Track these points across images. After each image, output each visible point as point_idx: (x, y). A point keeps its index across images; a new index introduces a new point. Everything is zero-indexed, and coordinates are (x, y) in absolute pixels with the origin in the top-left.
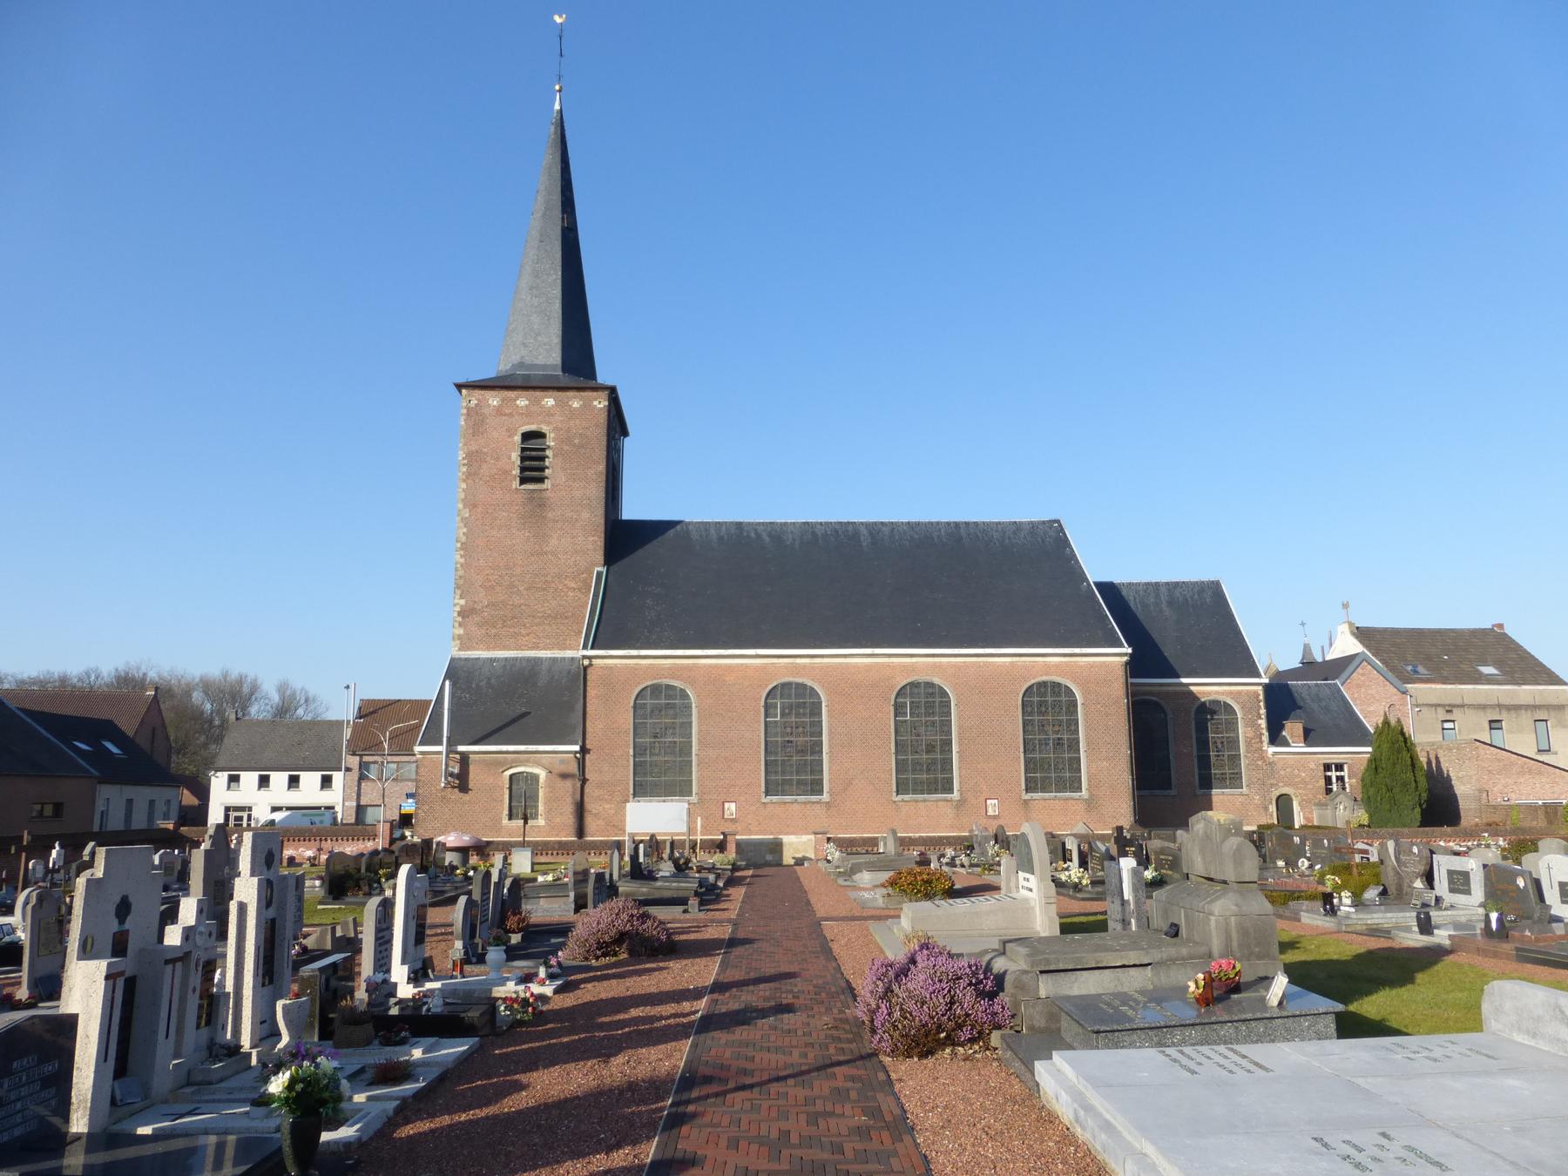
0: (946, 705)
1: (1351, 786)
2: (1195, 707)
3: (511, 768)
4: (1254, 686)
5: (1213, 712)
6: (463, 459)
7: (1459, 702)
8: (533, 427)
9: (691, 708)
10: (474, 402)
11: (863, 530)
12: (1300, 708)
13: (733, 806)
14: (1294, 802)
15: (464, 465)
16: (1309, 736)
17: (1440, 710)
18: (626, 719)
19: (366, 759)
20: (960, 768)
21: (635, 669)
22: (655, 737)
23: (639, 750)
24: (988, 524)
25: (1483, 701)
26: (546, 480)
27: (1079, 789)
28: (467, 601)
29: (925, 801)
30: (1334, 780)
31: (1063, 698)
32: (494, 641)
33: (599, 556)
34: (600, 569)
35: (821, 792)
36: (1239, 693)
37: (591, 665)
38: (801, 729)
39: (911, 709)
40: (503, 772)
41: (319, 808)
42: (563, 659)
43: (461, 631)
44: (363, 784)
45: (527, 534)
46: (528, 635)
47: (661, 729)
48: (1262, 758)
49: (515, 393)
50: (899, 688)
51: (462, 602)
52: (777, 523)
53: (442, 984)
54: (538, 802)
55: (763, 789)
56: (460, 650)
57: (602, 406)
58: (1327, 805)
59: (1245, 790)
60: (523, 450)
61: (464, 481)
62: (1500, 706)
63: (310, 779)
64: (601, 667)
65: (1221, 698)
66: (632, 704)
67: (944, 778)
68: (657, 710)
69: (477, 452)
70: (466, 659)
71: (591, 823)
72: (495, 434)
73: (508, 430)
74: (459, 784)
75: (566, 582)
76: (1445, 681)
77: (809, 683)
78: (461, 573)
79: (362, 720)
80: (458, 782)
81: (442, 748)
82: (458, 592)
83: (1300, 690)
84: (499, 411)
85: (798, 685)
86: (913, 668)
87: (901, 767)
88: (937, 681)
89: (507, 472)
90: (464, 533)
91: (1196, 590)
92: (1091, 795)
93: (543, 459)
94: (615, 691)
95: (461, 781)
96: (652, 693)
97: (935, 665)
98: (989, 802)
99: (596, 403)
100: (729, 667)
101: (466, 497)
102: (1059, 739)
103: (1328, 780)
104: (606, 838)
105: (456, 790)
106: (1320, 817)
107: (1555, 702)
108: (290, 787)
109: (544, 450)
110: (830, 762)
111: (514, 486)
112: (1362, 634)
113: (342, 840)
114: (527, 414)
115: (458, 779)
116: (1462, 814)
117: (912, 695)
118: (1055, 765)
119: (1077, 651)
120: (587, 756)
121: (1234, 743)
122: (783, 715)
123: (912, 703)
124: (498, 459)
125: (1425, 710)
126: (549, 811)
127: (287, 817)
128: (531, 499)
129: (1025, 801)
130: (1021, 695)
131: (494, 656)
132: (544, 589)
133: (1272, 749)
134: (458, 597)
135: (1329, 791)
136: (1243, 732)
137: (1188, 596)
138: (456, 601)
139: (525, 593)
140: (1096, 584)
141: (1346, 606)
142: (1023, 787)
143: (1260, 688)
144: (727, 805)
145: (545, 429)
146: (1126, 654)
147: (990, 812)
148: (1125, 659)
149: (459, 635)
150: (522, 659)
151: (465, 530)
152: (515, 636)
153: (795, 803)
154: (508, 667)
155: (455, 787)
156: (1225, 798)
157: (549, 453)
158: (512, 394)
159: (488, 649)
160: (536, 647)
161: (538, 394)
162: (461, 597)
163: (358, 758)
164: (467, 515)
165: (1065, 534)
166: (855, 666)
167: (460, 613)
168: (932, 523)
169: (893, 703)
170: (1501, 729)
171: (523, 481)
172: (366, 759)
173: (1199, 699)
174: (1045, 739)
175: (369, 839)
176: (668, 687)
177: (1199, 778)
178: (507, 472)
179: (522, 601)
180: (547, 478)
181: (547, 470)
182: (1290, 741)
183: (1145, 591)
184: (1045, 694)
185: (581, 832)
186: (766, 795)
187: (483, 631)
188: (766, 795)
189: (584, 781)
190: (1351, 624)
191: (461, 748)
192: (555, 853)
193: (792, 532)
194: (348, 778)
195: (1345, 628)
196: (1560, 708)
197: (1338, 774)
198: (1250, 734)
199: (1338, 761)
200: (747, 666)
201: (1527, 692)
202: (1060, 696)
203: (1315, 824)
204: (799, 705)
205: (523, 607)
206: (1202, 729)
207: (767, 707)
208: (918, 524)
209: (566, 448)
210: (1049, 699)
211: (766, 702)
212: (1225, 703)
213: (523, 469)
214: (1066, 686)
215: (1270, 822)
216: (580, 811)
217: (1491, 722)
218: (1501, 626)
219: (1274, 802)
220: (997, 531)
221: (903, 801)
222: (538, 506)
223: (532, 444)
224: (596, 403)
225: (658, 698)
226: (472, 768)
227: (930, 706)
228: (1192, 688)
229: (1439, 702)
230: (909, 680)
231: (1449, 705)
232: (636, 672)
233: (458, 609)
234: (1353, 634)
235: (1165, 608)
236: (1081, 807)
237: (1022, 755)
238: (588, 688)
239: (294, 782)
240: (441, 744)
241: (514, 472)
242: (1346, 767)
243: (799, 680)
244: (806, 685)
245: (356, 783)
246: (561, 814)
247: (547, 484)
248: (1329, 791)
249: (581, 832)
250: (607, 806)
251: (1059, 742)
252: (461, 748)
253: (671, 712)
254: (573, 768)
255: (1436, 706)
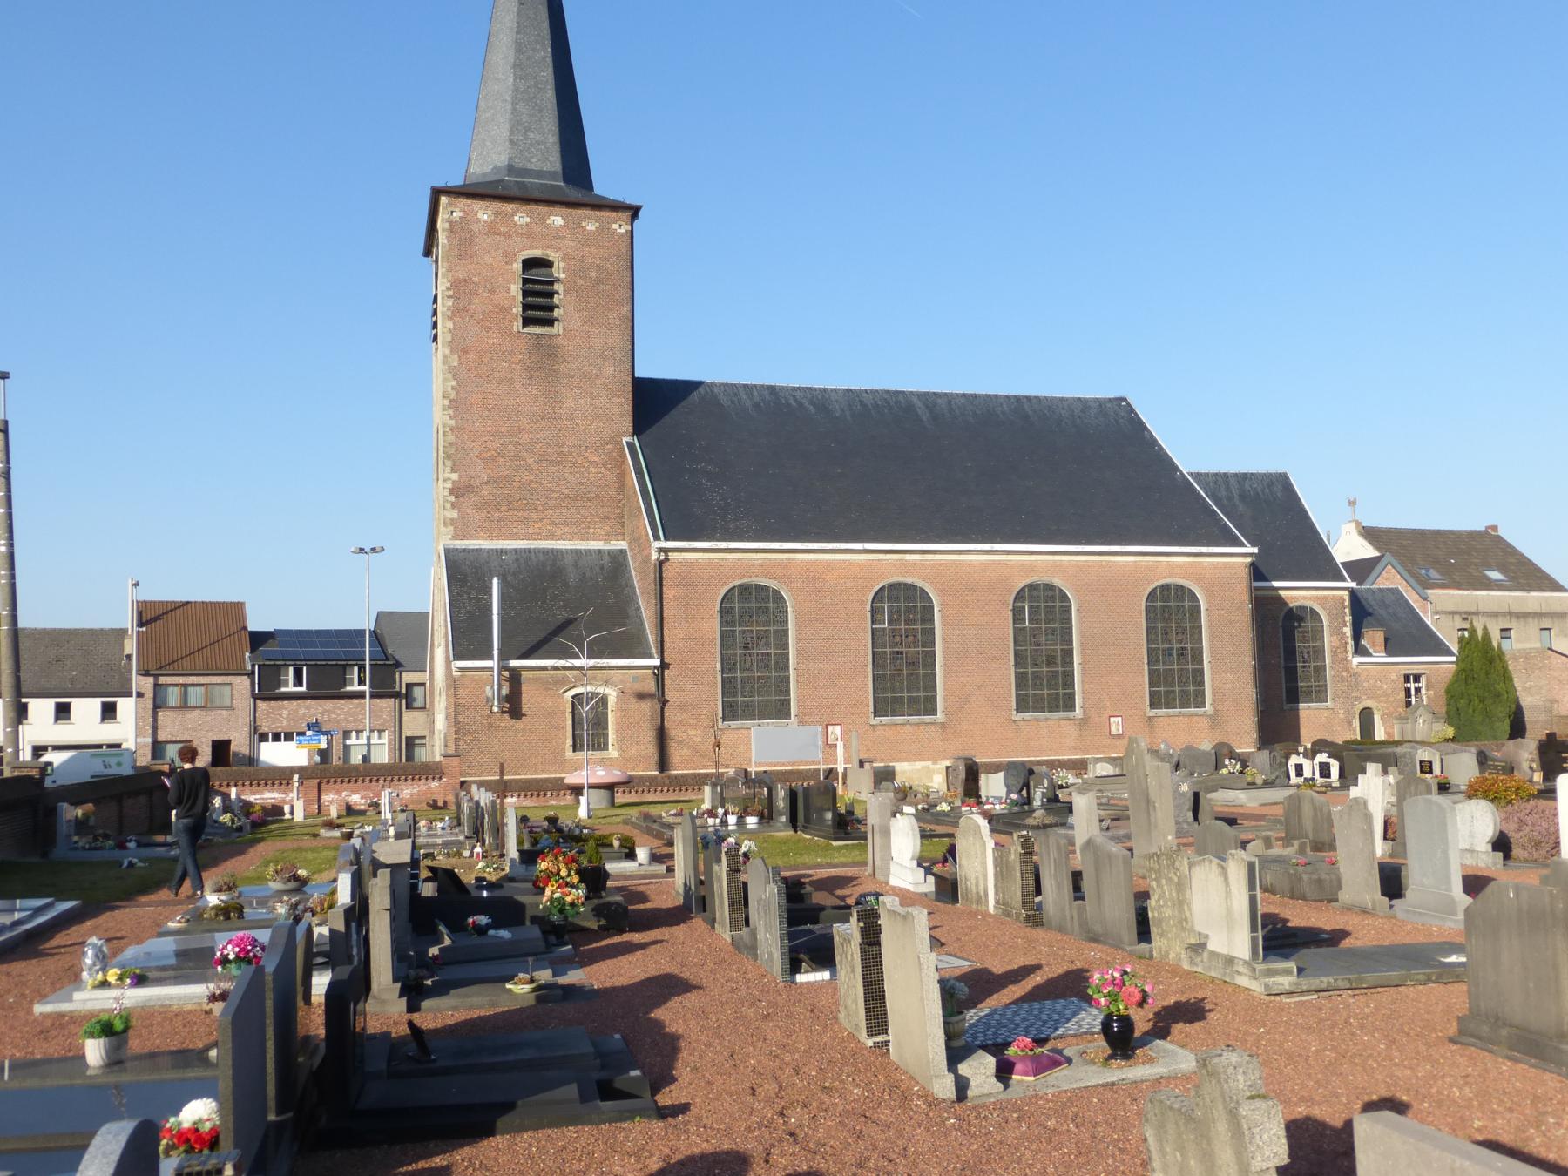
0: (1067, 610)
1: (1428, 697)
2: (1283, 614)
3: (574, 687)
4: (1340, 590)
5: (1301, 619)
6: (448, 289)
7: (1473, 609)
8: (537, 253)
9: (787, 612)
10: (457, 215)
11: (918, 403)
12: (1370, 614)
13: (837, 729)
14: (1375, 717)
15: (449, 297)
16: (1392, 647)
17: (1457, 618)
18: (712, 627)
19: (162, 680)
20: (1083, 681)
21: (720, 564)
22: (746, 648)
23: (728, 665)
24: (1052, 400)
25: (1495, 609)
26: (556, 323)
27: (1202, 704)
28: (460, 476)
29: (1046, 719)
30: (1413, 692)
31: (1187, 604)
32: (498, 528)
33: (627, 423)
34: (629, 439)
35: (934, 712)
36: (1326, 598)
37: (667, 559)
38: (911, 638)
39: (1030, 614)
40: (564, 693)
41: (100, 746)
42: (588, 552)
43: (454, 514)
44: (160, 714)
45: (534, 392)
46: (541, 520)
47: (752, 638)
48: (1347, 669)
49: (512, 205)
50: (1017, 590)
51: (455, 476)
52: (816, 389)
53: (70, 999)
54: (607, 729)
55: (871, 709)
56: (454, 538)
57: (623, 230)
58: (1407, 719)
59: (1330, 703)
60: (525, 281)
61: (450, 318)
62: (1510, 614)
63: (86, 709)
64: (680, 563)
65: (1308, 604)
66: (718, 608)
67: (780, 700)
68: (746, 615)
69: (465, 281)
70: (464, 550)
71: (677, 754)
72: (488, 259)
73: (505, 254)
74: (509, 708)
75: (586, 455)
76: (1459, 586)
77: (920, 584)
78: (451, 438)
79: (144, 629)
80: (508, 705)
81: (493, 663)
82: (449, 463)
83: (1365, 596)
84: (491, 229)
85: (907, 585)
86: (1031, 567)
87: (1021, 681)
88: (1057, 582)
89: (506, 310)
90: (453, 388)
91: (1265, 483)
92: (1216, 711)
93: (551, 294)
94: (696, 592)
95: (513, 706)
96: (741, 594)
97: (1055, 565)
98: (1112, 719)
99: (615, 226)
100: (830, 563)
101: (453, 339)
102: (1182, 648)
103: (1408, 691)
104: (691, 771)
105: (507, 716)
106: (1402, 731)
107: (1558, 609)
108: (57, 719)
109: (551, 283)
110: (945, 676)
111: (515, 329)
112: (1370, 534)
113: (399, 780)
114: (529, 235)
115: (507, 702)
116: (1528, 726)
117: (1031, 599)
118: (1179, 678)
119: (1204, 550)
120: (667, 672)
121: (1319, 652)
122: (891, 622)
123: (1030, 607)
124: (492, 292)
125: (1443, 617)
126: (621, 740)
127: (73, 757)
128: (538, 346)
129: (1149, 718)
130: (1144, 599)
131: (499, 547)
132: (560, 463)
133: (1357, 660)
134: (448, 470)
135: (1408, 704)
136: (1328, 641)
137: (1259, 489)
138: (447, 475)
139: (536, 466)
140: (1191, 474)
141: (1352, 503)
142: (1148, 703)
143: (1346, 592)
144: (830, 728)
145: (552, 255)
146: (1251, 555)
147: (1114, 732)
148: (1249, 560)
149: (452, 520)
150: (537, 551)
151: (454, 383)
152: (524, 521)
153: (906, 725)
154: (522, 561)
155: (505, 712)
156: (1311, 712)
157: (556, 287)
158: (508, 207)
159: (491, 538)
160: (551, 536)
161: (542, 209)
162: (453, 471)
163: (151, 680)
164: (456, 364)
165: (1136, 414)
166: (970, 564)
167: (452, 491)
168: (989, 396)
169: (1011, 607)
170: (1510, 638)
171: (527, 322)
172: (162, 680)
173: (1287, 604)
174: (1169, 649)
175: (434, 779)
176: (760, 588)
177: (1287, 692)
178: (506, 310)
179: (532, 478)
180: (558, 320)
181: (556, 310)
182: (1371, 651)
183: (1215, 483)
184: (1167, 599)
185: (663, 764)
186: (875, 716)
187: (483, 515)
188: (875, 716)
189: (664, 702)
190: (1358, 523)
191: (514, 663)
192: (665, 789)
193: (837, 401)
194: (139, 705)
195: (1352, 527)
196: (1561, 616)
197: (1417, 685)
198: (1336, 644)
199: (1415, 672)
200: (851, 563)
201: (1534, 599)
202: (1183, 601)
203: (1396, 739)
204: (908, 610)
205: (533, 485)
206: (1289, 638)
207: (874, 611)
208: (975, 396)
209: (580, 282)
210: (1173, 604)
211: (872, 607)
212: (1311, 609)
213: (526, 307)
214: (1190, 590)
215: (1353, 737)
216: (662, 736)
217: (1502, 630)
218: (1495, 528)
219: (1357, 716)
220: (1063, 409)
221: (1024, 720)
222: (547, 355)
223: (536, 274)
224: (615, 226)
225: (748, 600)
226: (524, 687)
227: (1050, 610)
228: (1281, 592)
229: (1455, 609)
230: (1028, 581)
231: (1466, 613)
232: (722, 569)
233: (449, 485)
234: (1360, 534)
235: (1237, 503)
236: (1205, 723)
237: (1146, 666)
238: (664, 589)
239: (63, 712)
240: (491, 658)
241: (515, 310)
242: (1423, 679)
243: (909, 580)
244: (915, 586)
245: (150, 713)
246: (637, 744)
247: (558, 328)
248: (1408, 704)
249: (663, 764)
250: (692, 733)
251: (1182, 653)
252: (514, 663)
253: (763, 618)
254: (651, 686)
255: (1454, 613)
